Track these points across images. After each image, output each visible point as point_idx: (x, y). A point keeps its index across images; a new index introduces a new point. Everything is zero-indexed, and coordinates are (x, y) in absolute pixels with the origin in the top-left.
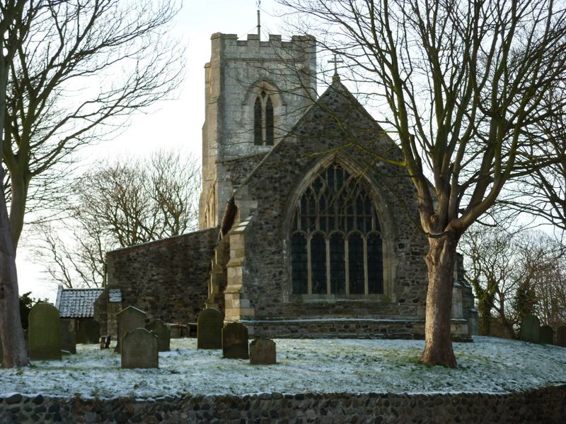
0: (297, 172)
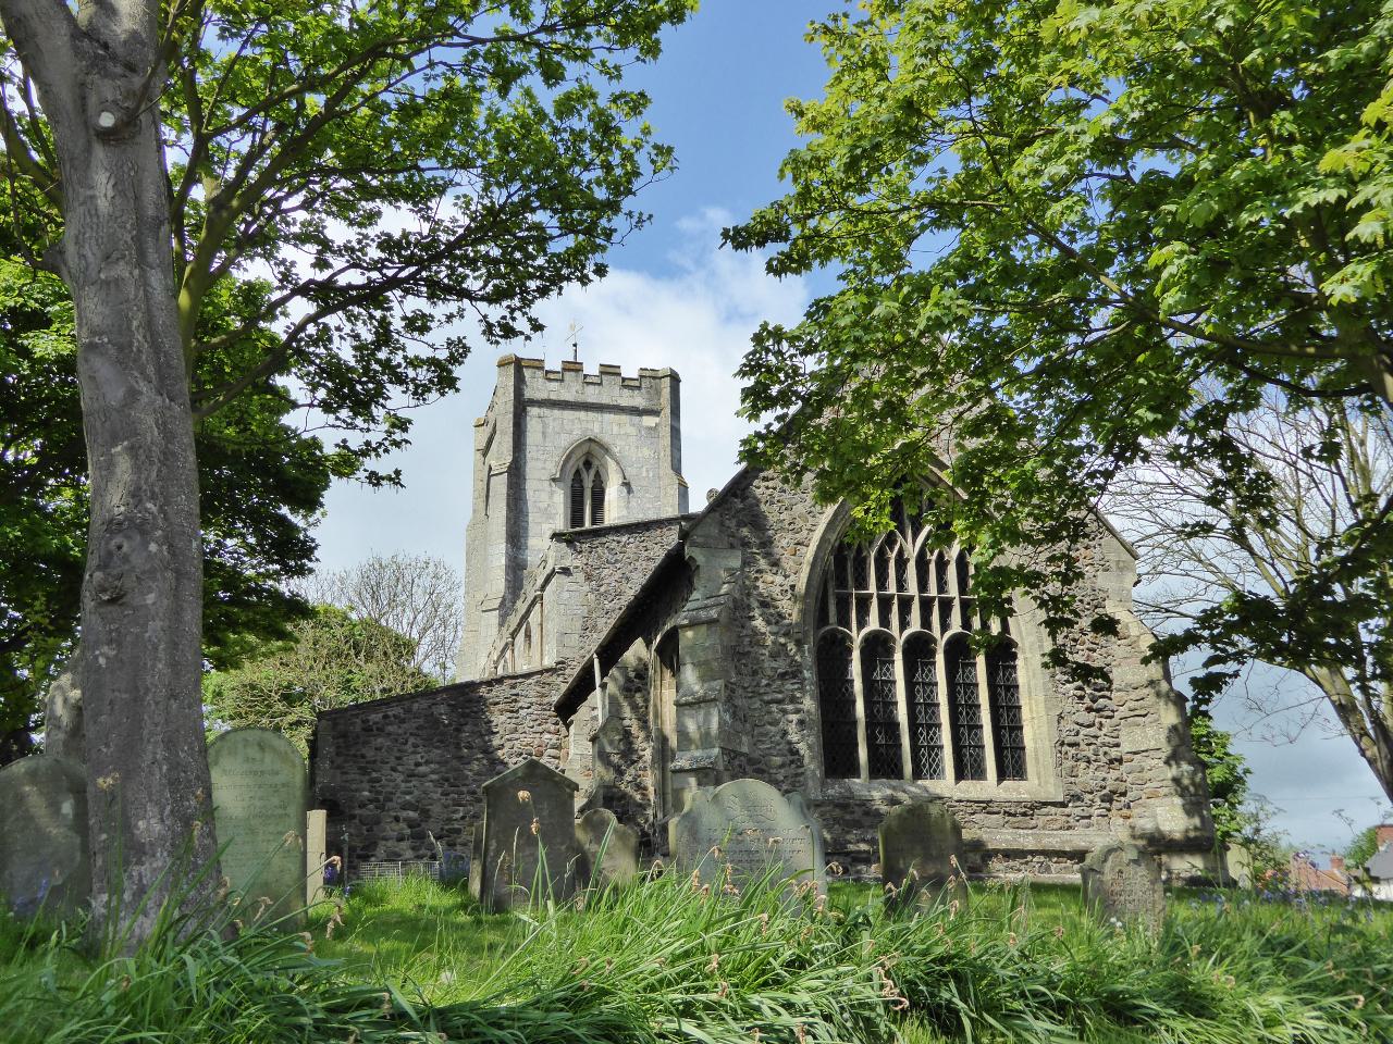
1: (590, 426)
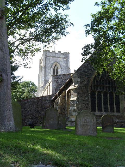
0: (92, 70)
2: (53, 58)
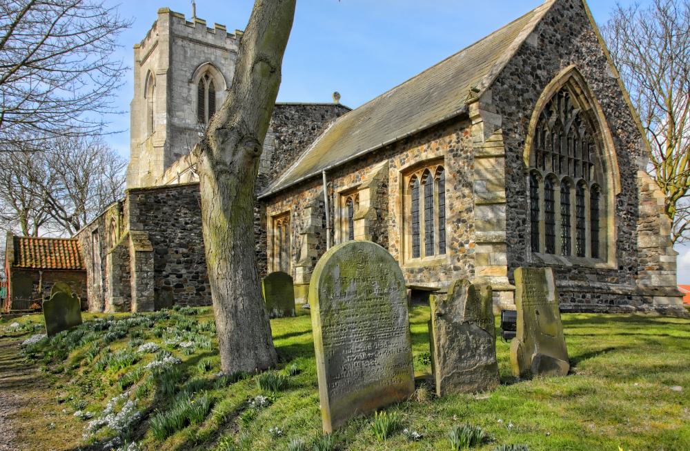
1: (209, 56)
2: (198, 46)
